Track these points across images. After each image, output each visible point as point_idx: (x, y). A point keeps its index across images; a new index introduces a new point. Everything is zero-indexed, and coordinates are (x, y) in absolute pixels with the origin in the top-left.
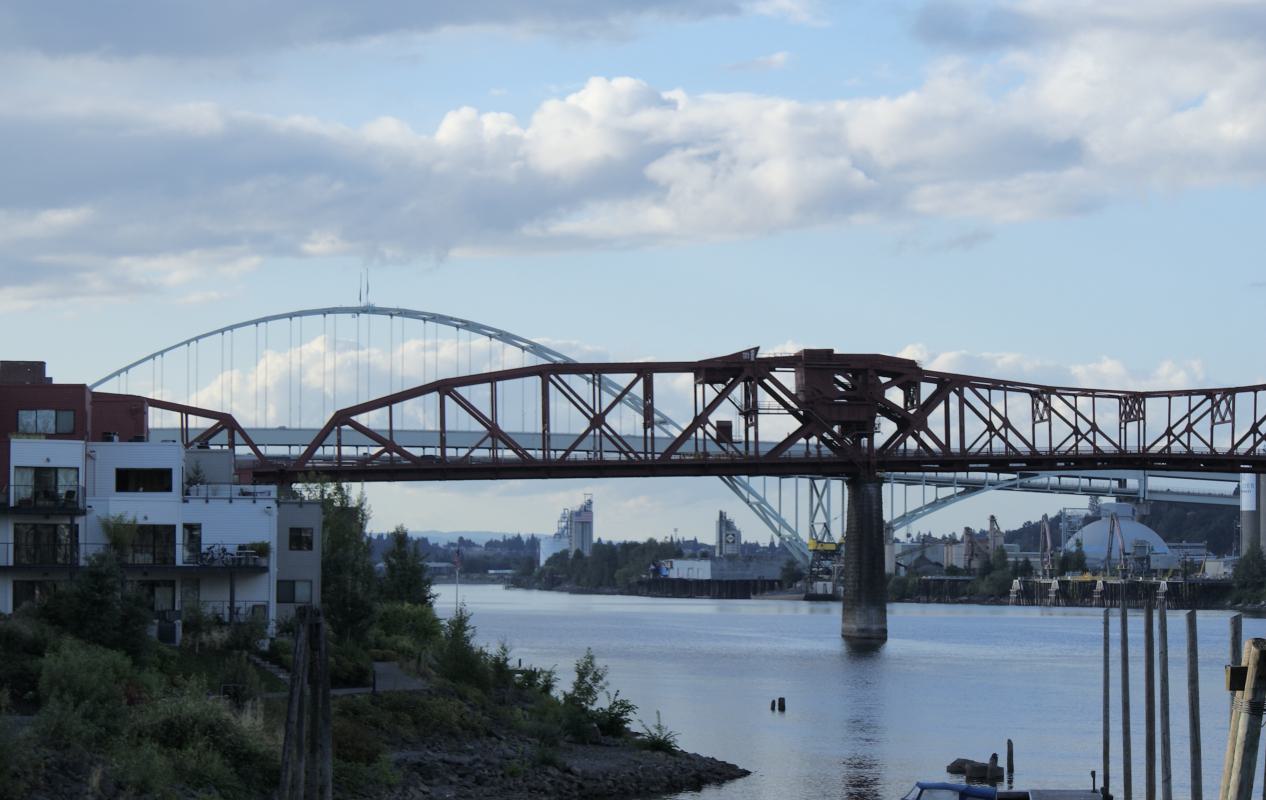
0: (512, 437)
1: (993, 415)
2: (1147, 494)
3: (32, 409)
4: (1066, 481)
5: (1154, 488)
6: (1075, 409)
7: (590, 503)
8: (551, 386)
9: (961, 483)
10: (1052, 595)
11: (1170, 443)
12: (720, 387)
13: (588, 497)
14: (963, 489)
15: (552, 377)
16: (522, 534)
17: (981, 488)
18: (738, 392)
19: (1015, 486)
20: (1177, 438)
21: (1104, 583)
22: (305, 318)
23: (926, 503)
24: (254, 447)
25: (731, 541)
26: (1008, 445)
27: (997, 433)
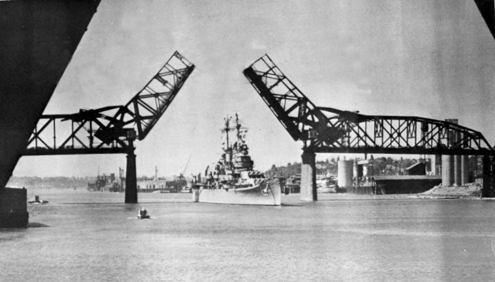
3: (423, 154)
4: (462, 174)
6: (391, 125)
8: (139, 105)
11: (392, 142)
12: (80, 123)
15: (139, 101)
18: (87, 124)
20: (395, 139)
26: (366, 144)
27: (362, 138)
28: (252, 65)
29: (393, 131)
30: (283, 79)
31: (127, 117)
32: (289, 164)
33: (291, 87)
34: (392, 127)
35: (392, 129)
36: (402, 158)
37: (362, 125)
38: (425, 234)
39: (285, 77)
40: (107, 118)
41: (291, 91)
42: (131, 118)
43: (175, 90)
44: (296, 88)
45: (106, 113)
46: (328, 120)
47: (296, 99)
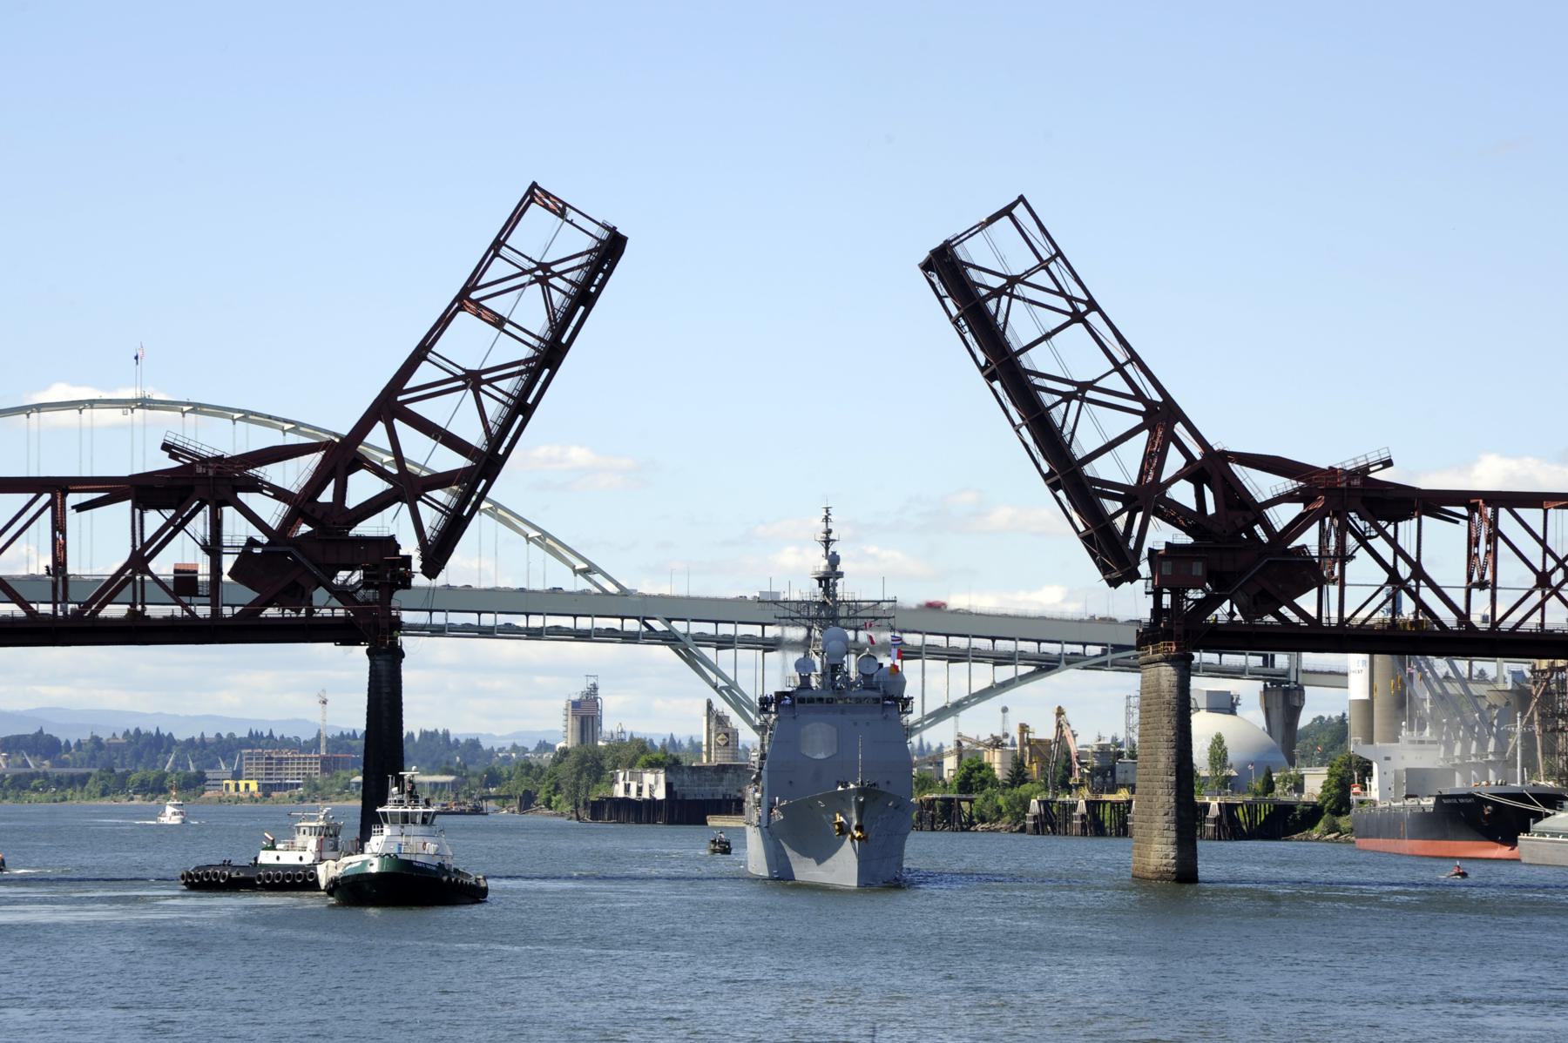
0: (11, 584)
1: (1400, 561)
2: (1300, 675)
5: (1310, 668)
6: (1543, 542)
7: (595, 688)
9: (1024, 658)
10: (1077, 822)
13: (592, 681)
14: (1032, 669)
16: (452, 732)
17: (1057, 667)
18: (199, 525)
19: (1105, 664)
21: (1045, 804)
22: (1118, 449)
23: (974, 691)
24: (24, 605)
25: (722, 743)
28: (959, 239)
29: (1551, 563)
30: (1086, 313)
31: (363, 486)
32: (219, 735)
33: (1121, 357)
34: (1547, 550)
35: (1548, 557)
36: (585, 713)
37: (1406, 531)
38: (1540, 1024)
39: (1092, 305)
40: (280, 494)
41: (1119, 368)
42: (378, 486)
43: (551, 354)
44: (1134, 358)
45: (273, 473)
46: (1255, 511)
47: (1140, 406)
